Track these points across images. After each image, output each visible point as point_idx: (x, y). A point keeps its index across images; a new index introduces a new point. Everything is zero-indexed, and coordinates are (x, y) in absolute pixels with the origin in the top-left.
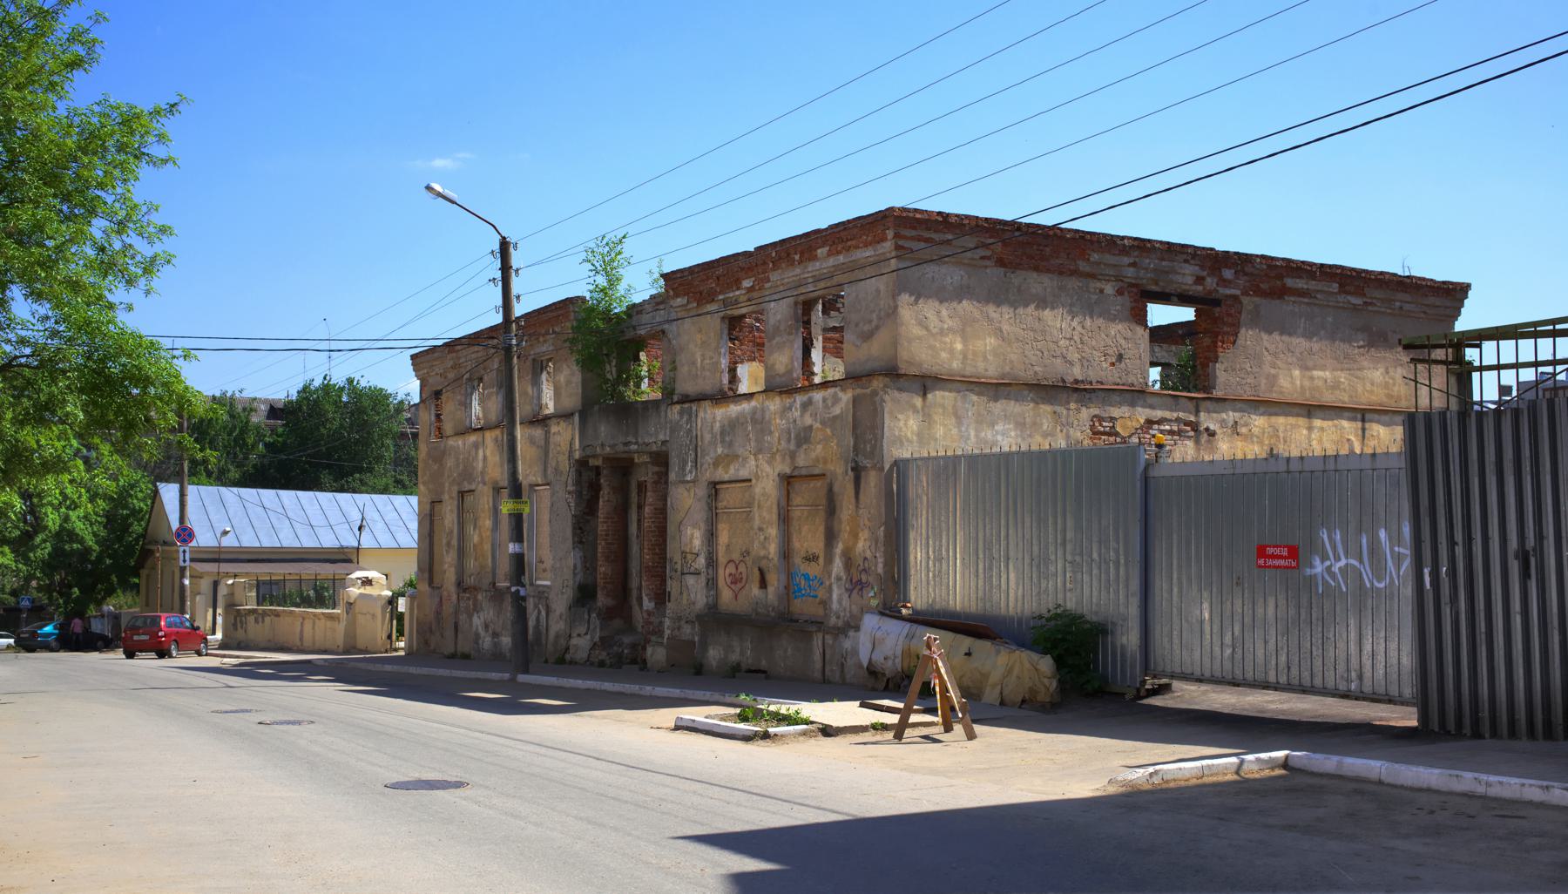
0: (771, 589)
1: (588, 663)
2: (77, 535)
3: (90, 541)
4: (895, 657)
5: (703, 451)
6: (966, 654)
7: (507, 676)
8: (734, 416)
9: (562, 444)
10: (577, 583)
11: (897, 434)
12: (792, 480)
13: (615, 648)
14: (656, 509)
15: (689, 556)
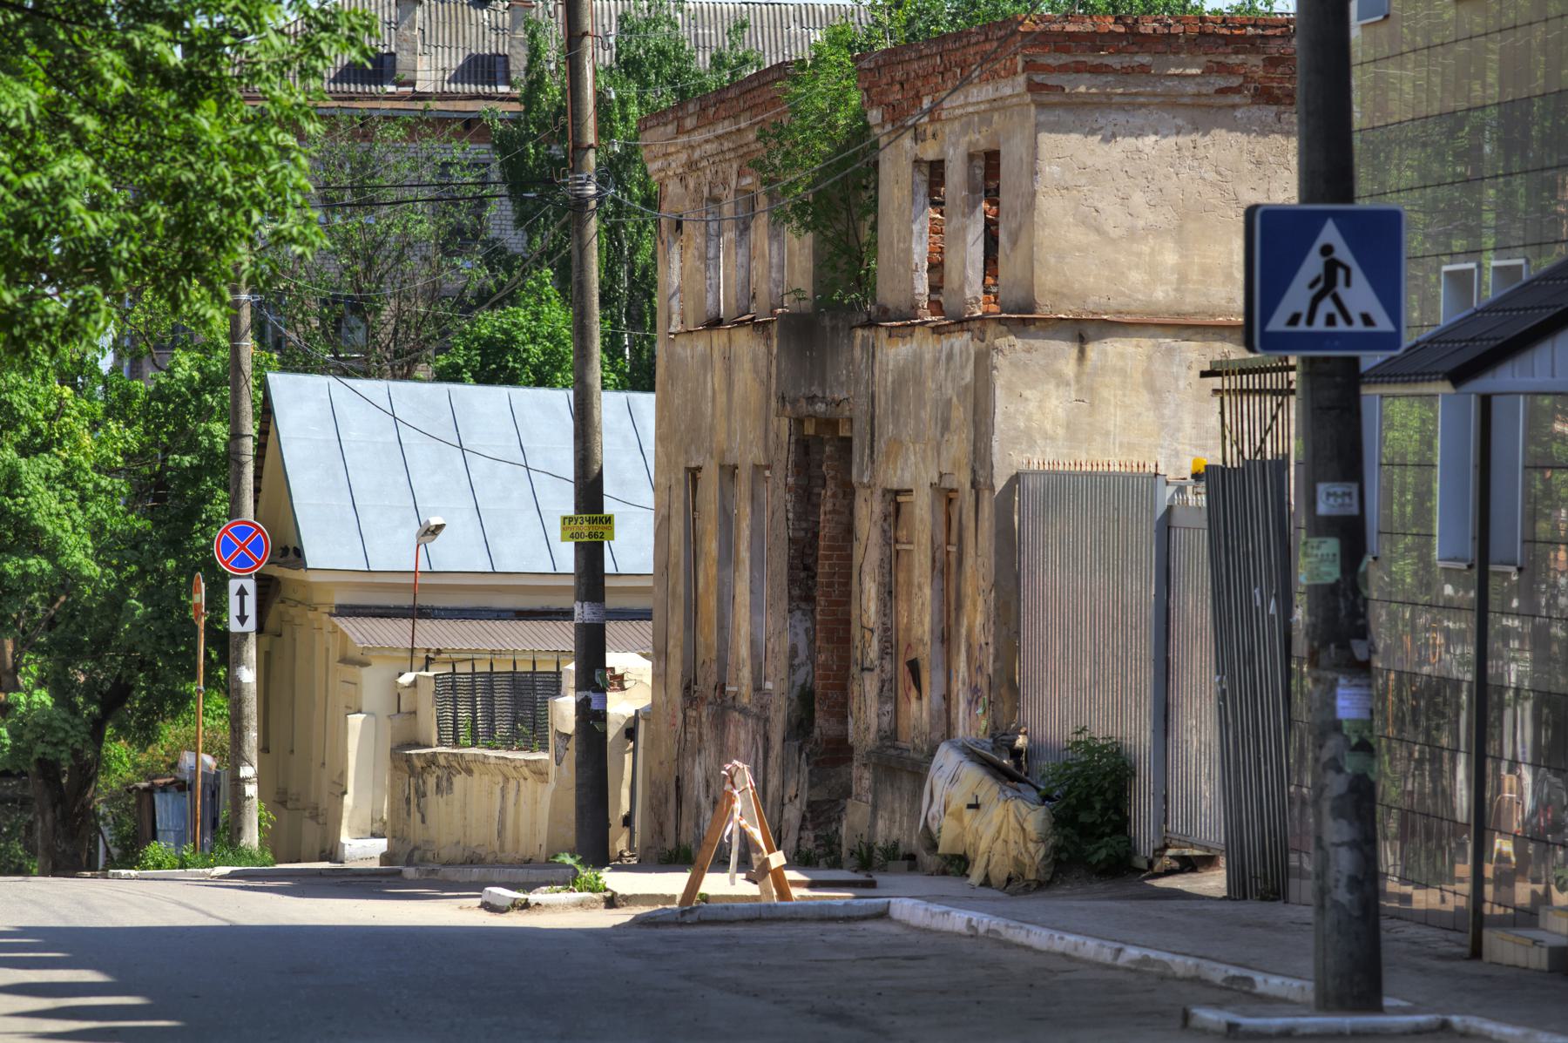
0: (925, 700)
2: (40, 531)
3: (80, 556)
6: (970, 806)
11: (1022, 425)
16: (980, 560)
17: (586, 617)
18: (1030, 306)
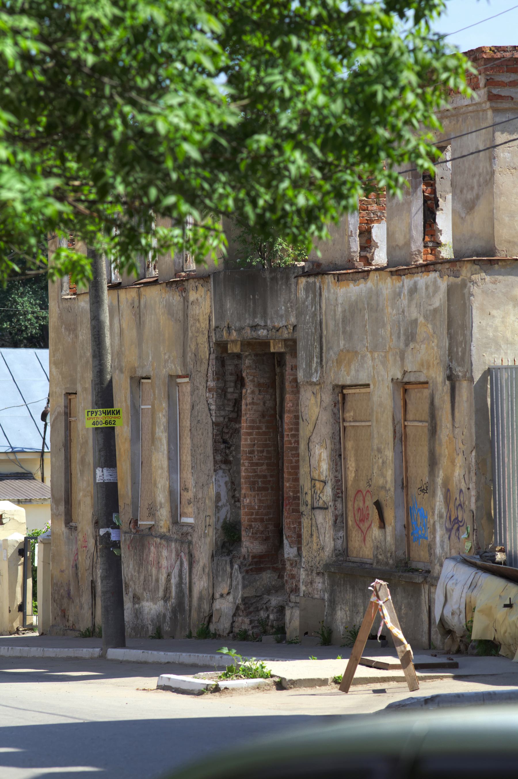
0: (389, 529)
1: (231, 635)
4: (460, 612)
5: (328, 342)
6: (506, 606)
7: (97, 651)
8: (353, 298)
9: (201, 318)
11: (491, 334)
12: (407, 387)
15: (318, 485)
16: (457, 431)
17: (106, 478)
18: (491, 251)
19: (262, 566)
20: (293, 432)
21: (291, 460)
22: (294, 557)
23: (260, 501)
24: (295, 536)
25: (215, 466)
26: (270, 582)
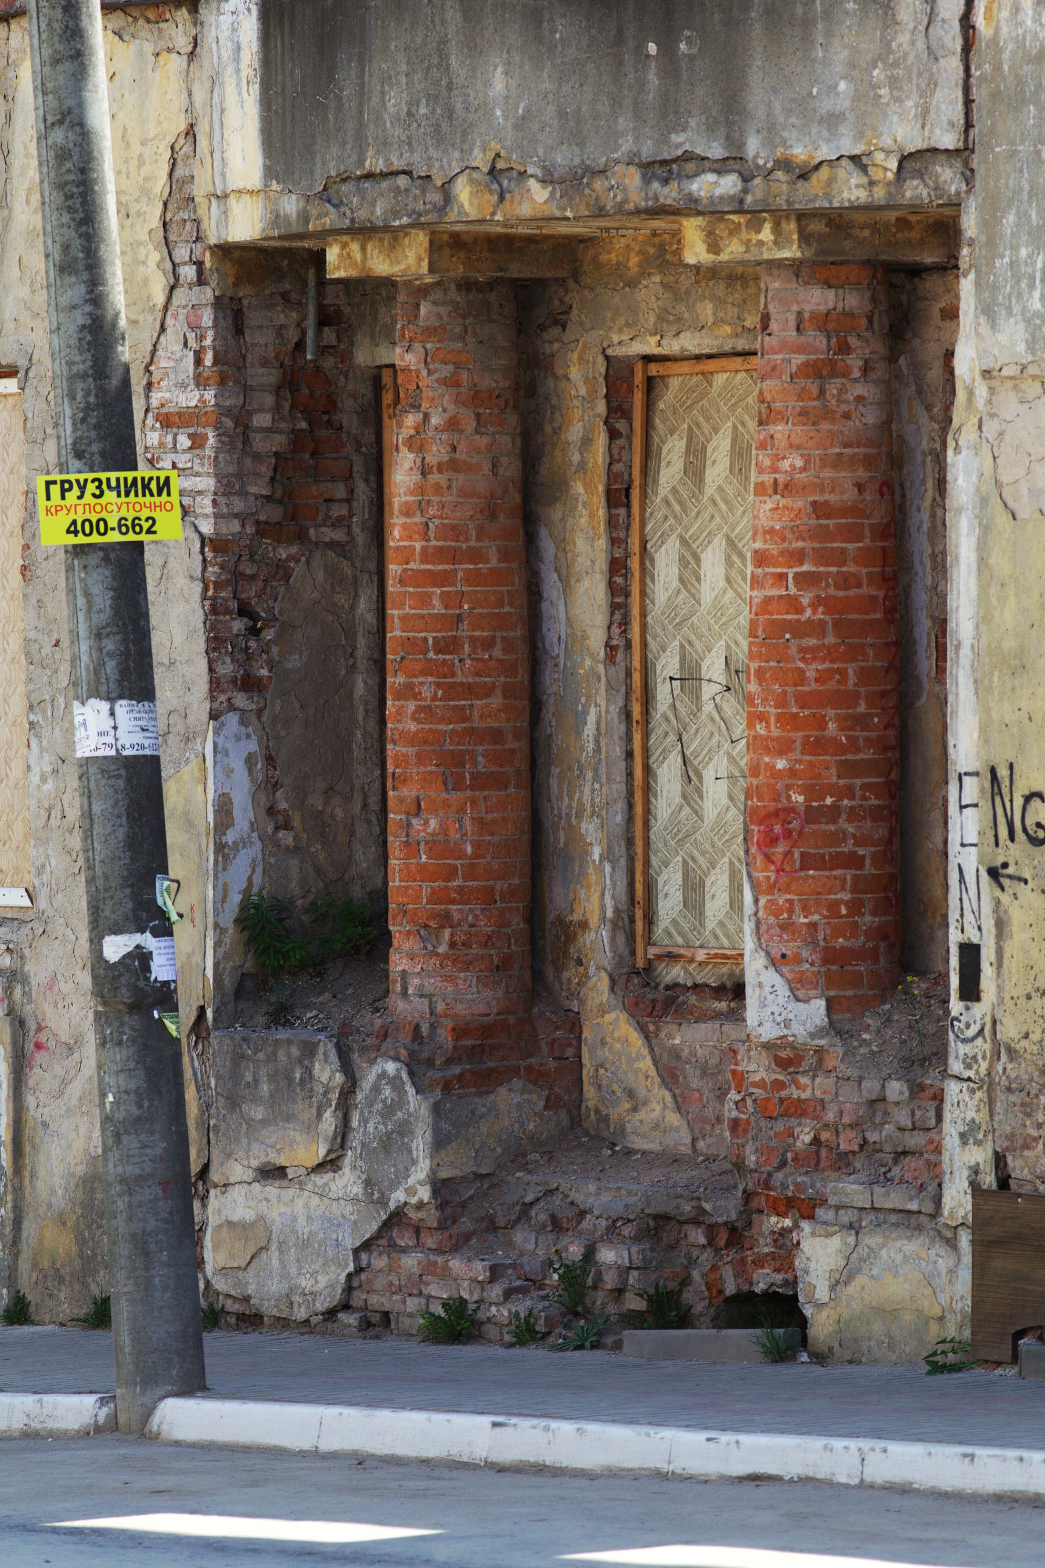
10: (236, 898)
13: (523, 1238)
14: (819, 509)
19: (491, 1064)
20: (806, 568)
21: (801, 672)
22: (812, 1036)
23: (481, 823)
24: (816, 957)
25: (213, 699)
26: (522, 1124)
